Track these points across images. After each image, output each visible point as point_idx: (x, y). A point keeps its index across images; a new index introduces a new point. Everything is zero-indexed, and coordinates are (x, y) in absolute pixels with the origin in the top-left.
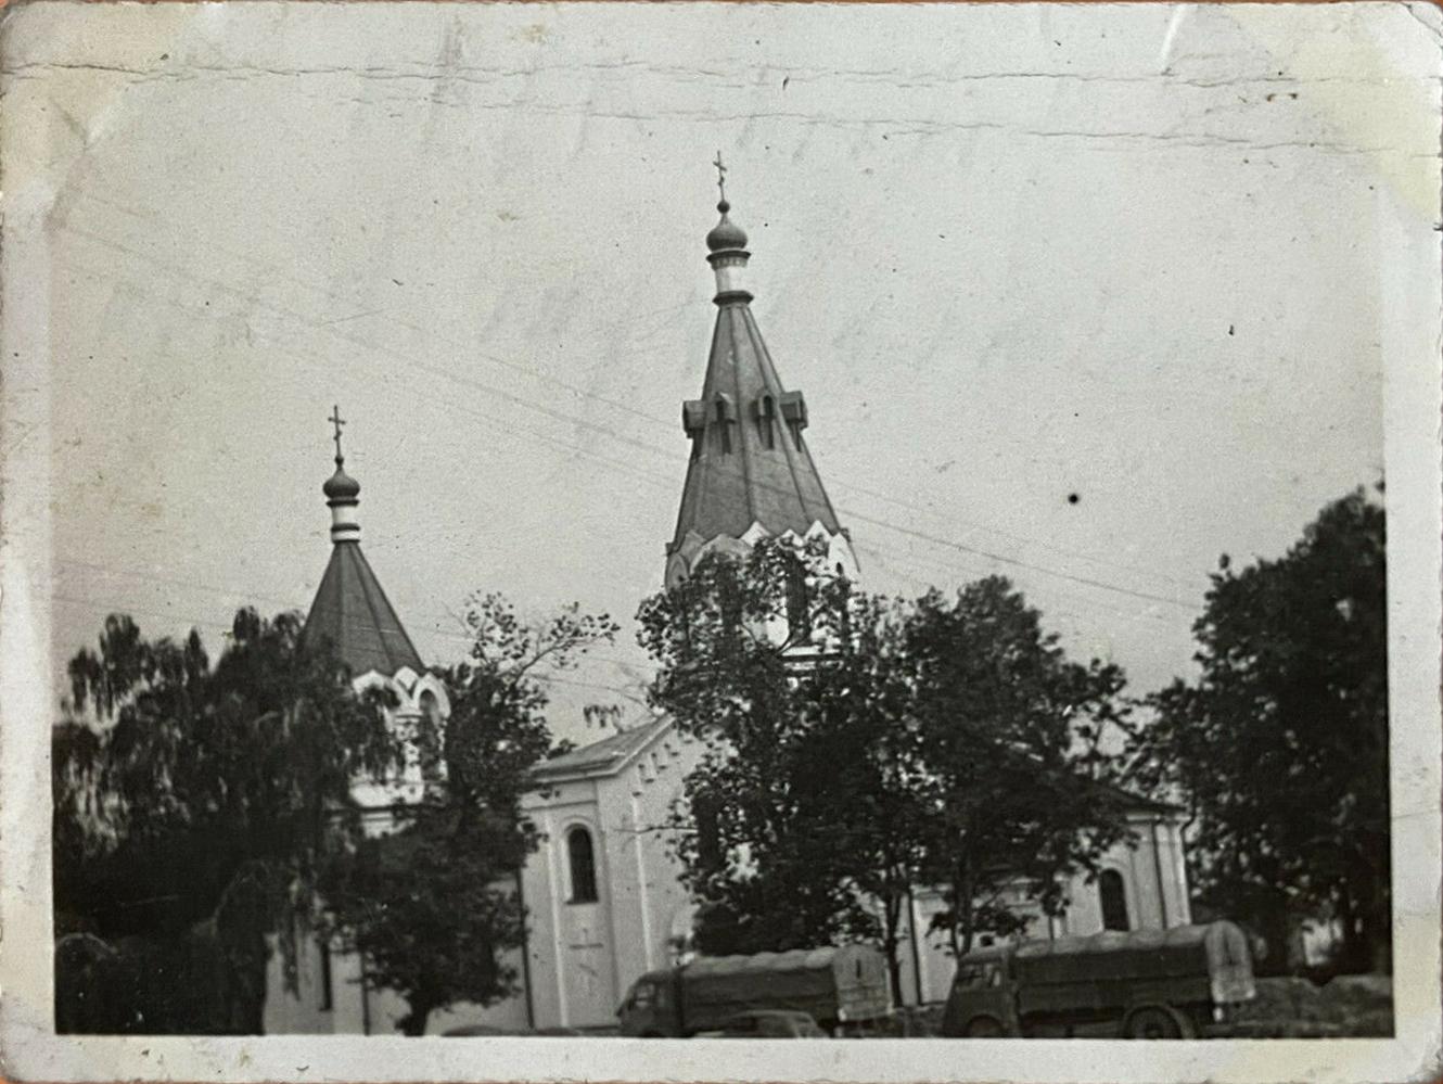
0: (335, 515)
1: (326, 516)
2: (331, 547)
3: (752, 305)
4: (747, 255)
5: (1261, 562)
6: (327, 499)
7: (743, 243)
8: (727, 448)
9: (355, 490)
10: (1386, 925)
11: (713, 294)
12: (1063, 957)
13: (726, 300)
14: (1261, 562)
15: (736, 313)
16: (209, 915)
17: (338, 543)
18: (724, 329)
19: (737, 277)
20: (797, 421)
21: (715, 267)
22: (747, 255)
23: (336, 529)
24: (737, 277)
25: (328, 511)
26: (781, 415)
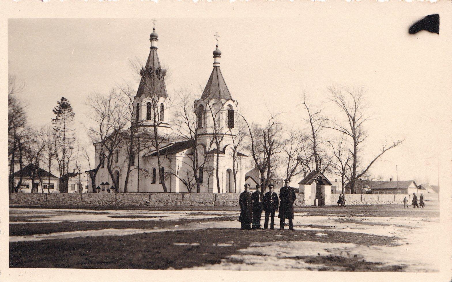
0: (215, 60)
1: (212, 60)
2: (213, 68)
3: (157, 50)
4: (158, 40)
5: (328, 243)
6: (213, 56)
7: (157, 37)
8: (151, 78)
9: (220, 54)
10: (60, 263)
11: (150, 47)
12: (83, 238)
13: (152, 48)
14: (328, 243)
15: (155, 51)
16: (280, 194)
17: (214, 67)
18: (152, 55)
19: (155, 44)
20: (164, 75)
21: (151, 41)
22: (158, 40)
23: (214, 63)
24: (155, 44)
25: (213, 59)
26: (160, 73)
